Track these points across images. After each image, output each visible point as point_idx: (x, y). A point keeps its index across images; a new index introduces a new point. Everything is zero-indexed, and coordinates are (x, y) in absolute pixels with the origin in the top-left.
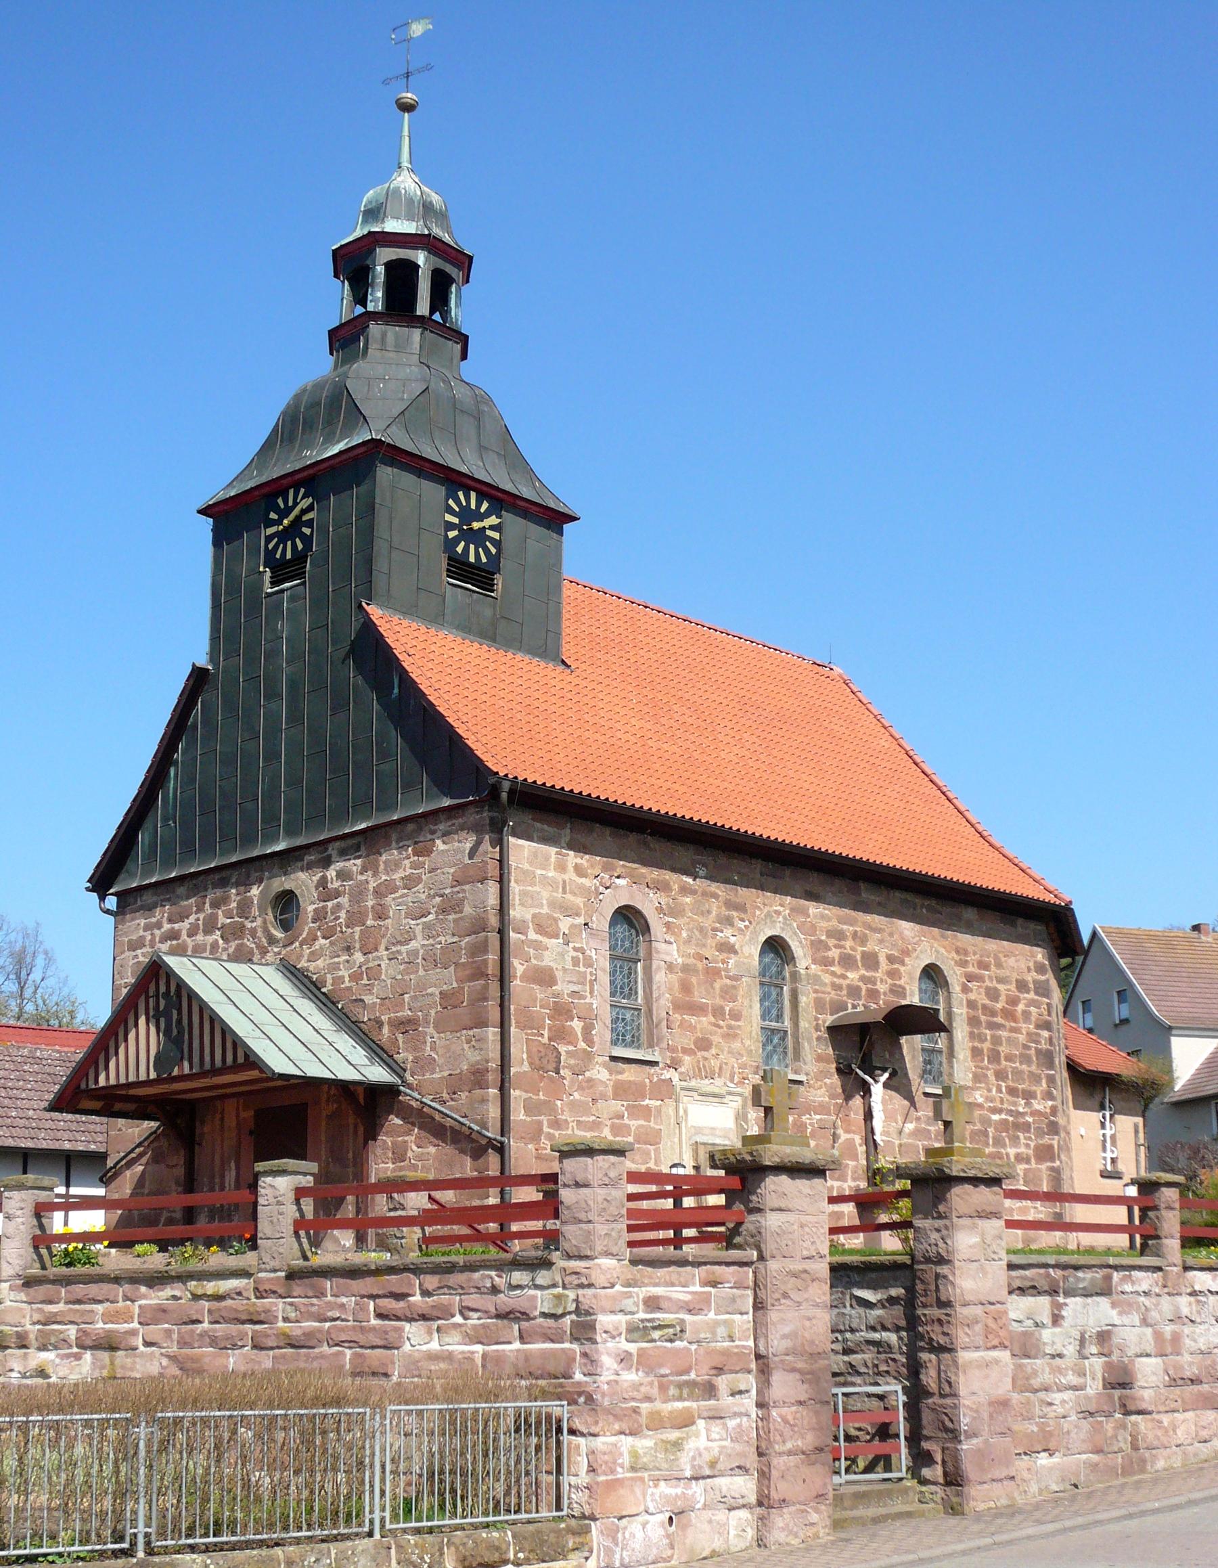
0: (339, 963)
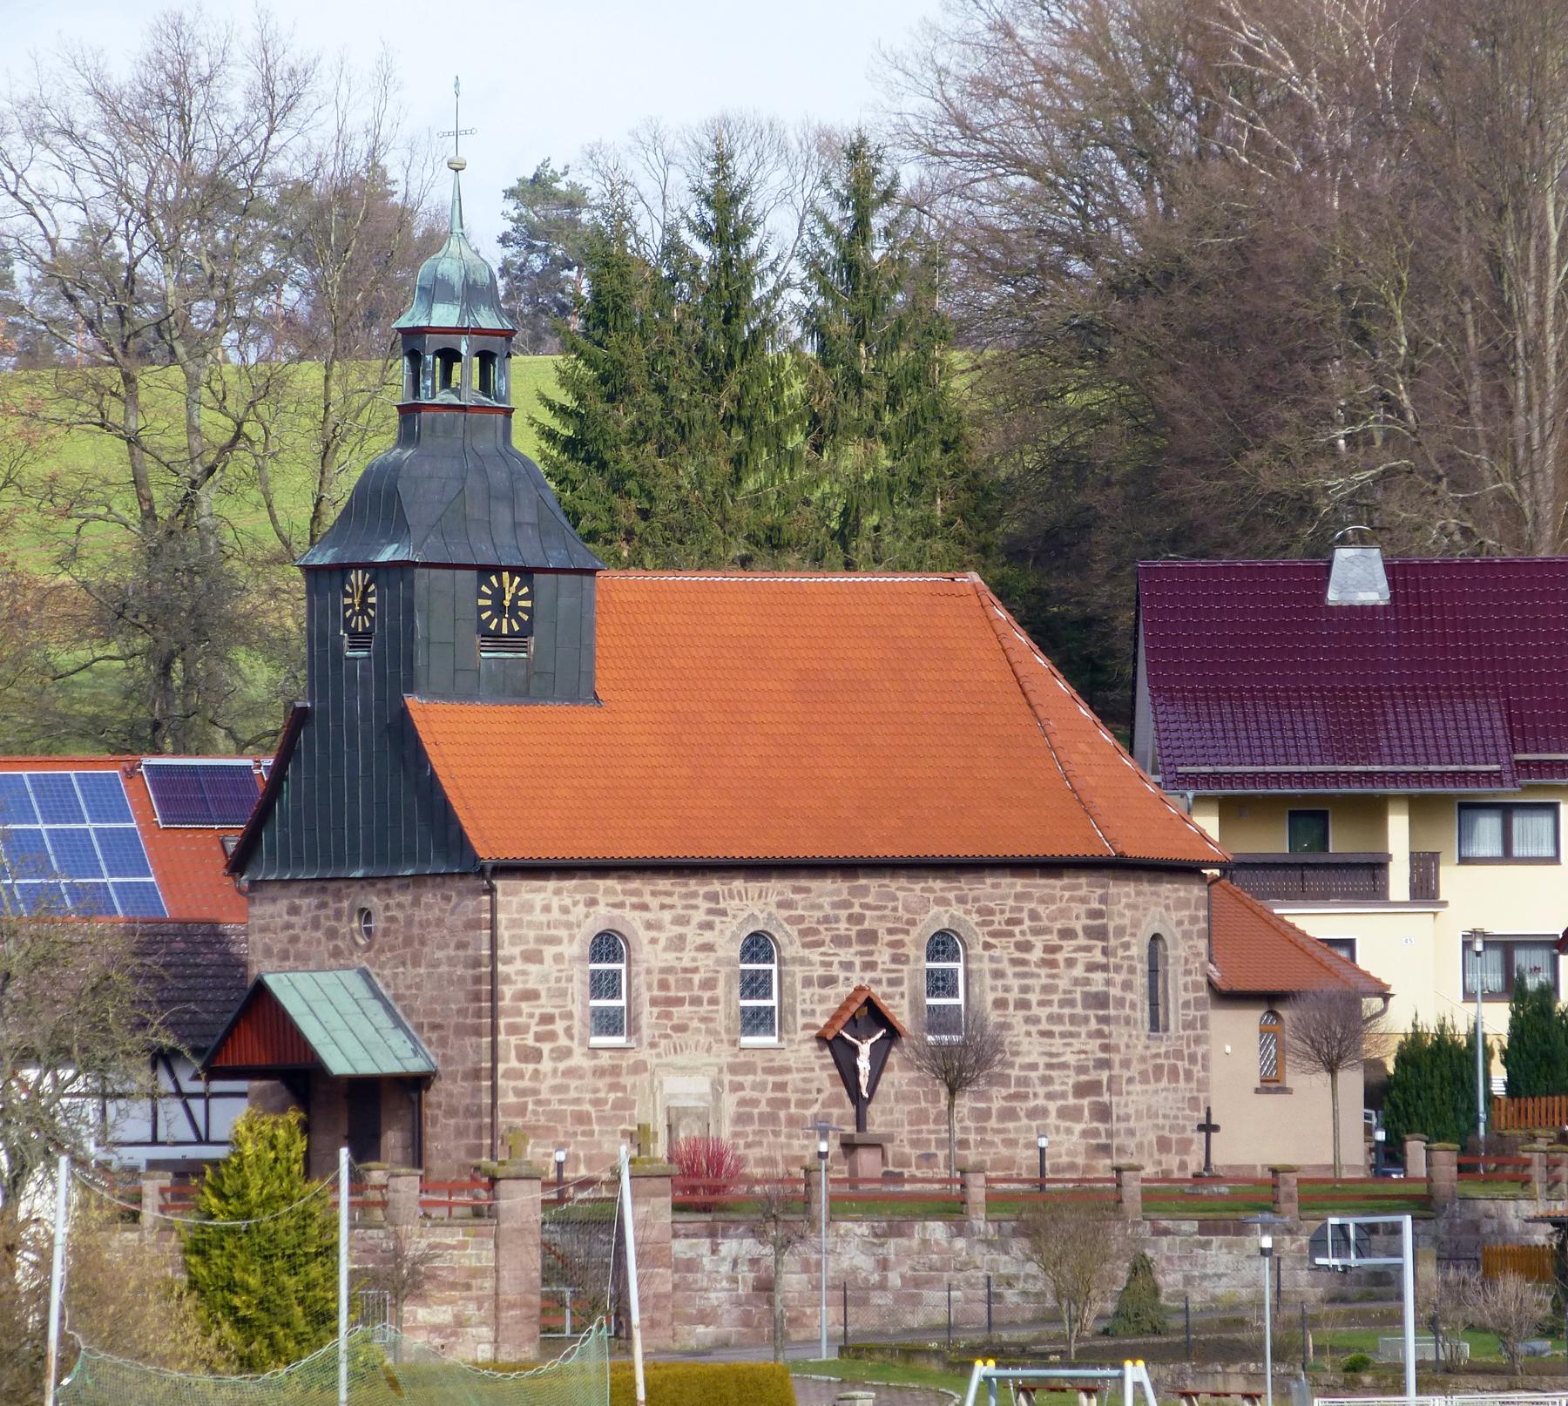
0: (1347, 423)
